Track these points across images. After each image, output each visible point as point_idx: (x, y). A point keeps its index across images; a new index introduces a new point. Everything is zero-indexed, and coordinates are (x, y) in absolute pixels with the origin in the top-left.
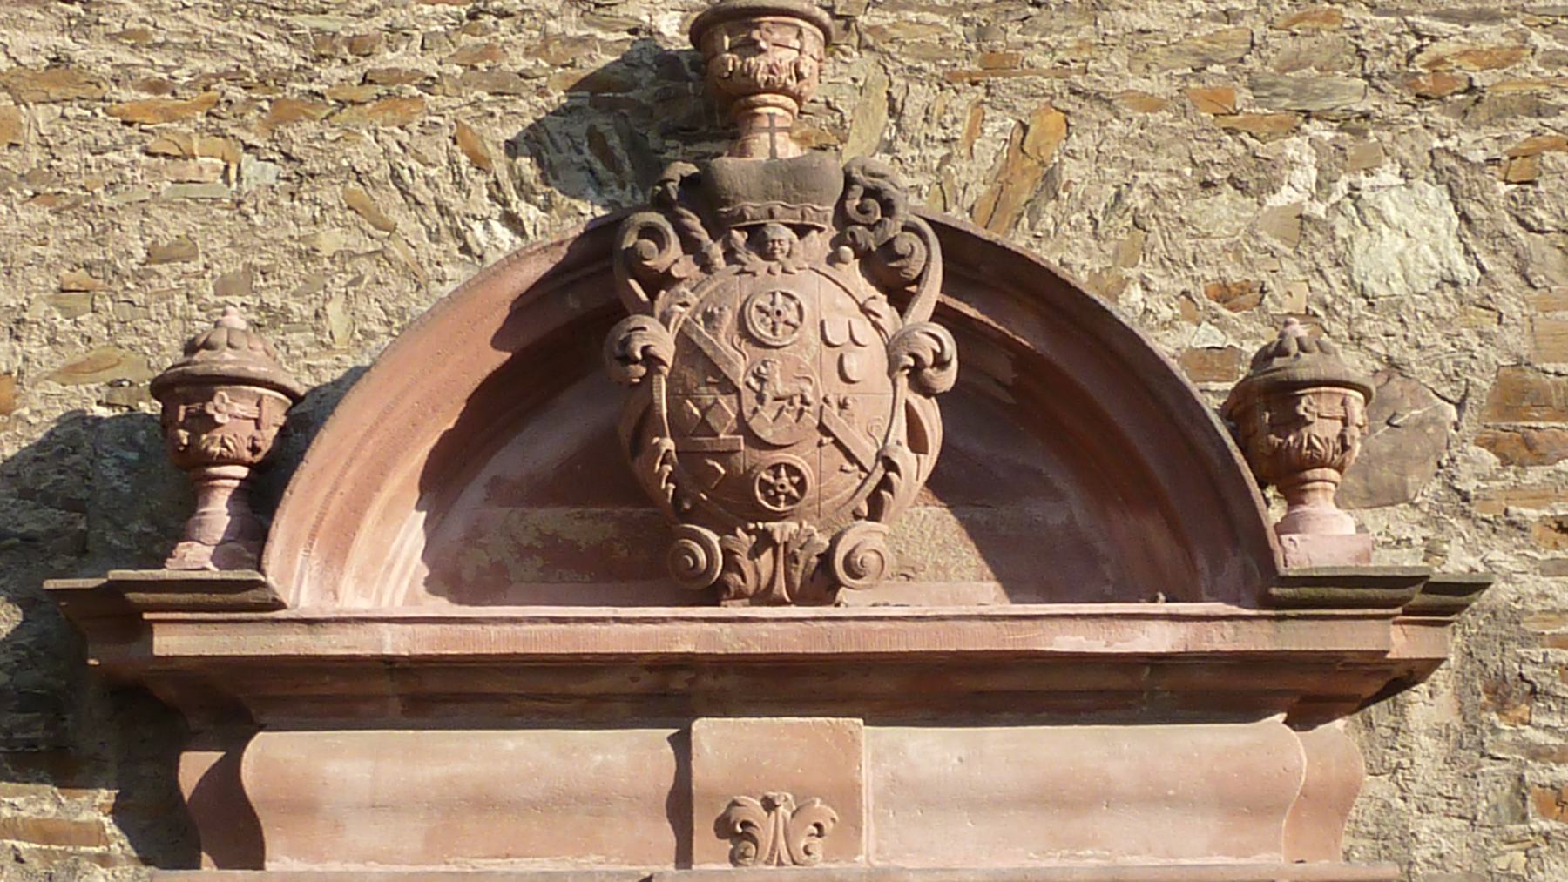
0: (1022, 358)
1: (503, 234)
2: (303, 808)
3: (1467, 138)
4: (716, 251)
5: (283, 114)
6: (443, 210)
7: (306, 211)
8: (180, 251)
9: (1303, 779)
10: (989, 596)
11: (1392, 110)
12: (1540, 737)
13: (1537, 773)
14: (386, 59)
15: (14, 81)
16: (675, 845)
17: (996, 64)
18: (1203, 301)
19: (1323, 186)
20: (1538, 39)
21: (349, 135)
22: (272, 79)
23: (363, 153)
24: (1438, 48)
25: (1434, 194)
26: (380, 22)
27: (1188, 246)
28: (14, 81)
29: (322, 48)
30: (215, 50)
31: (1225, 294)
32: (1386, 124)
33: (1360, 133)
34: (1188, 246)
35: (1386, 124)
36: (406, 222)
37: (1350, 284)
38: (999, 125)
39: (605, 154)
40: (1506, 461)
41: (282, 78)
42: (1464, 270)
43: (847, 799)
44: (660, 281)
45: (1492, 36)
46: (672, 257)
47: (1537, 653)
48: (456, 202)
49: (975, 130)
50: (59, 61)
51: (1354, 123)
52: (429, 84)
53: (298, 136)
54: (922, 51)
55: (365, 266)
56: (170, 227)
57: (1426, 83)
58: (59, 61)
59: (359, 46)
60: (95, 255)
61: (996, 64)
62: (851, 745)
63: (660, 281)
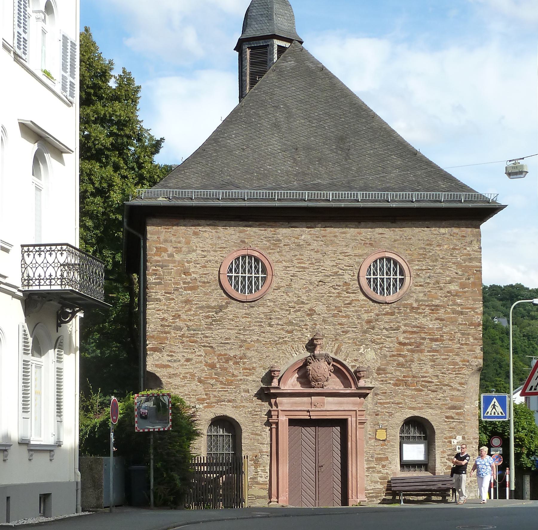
1: (295, 355)
2: (281, 403)
4: (315, 360)
5: (276, 344)
8: (268, 356)
10: (342, 387)
11: (370, 344)
13: (378, 401)
14: (285, 339)
17: (336, 340)
19: (364, 351)
21: (282, 346)
22: (276, 341)
23: (283, 348)
25: (373, 351)
29: (280, 338)
31: (355, 360)
38: (337, 345)
39: (304, 348)
41: (276, 341)
42: (375, 358)
43: (324, 403)
44: (310, 363)
45: (379, 337)
46: (311, 361)
48: (291, 352)
50: (258, 339)
51: (367, 345)
52: (289, 341)
54: (330, 338)
56: (267, 354)
58: (258, 339)
59: (283, 338)
62: (324, 399)
63: (310, 363)
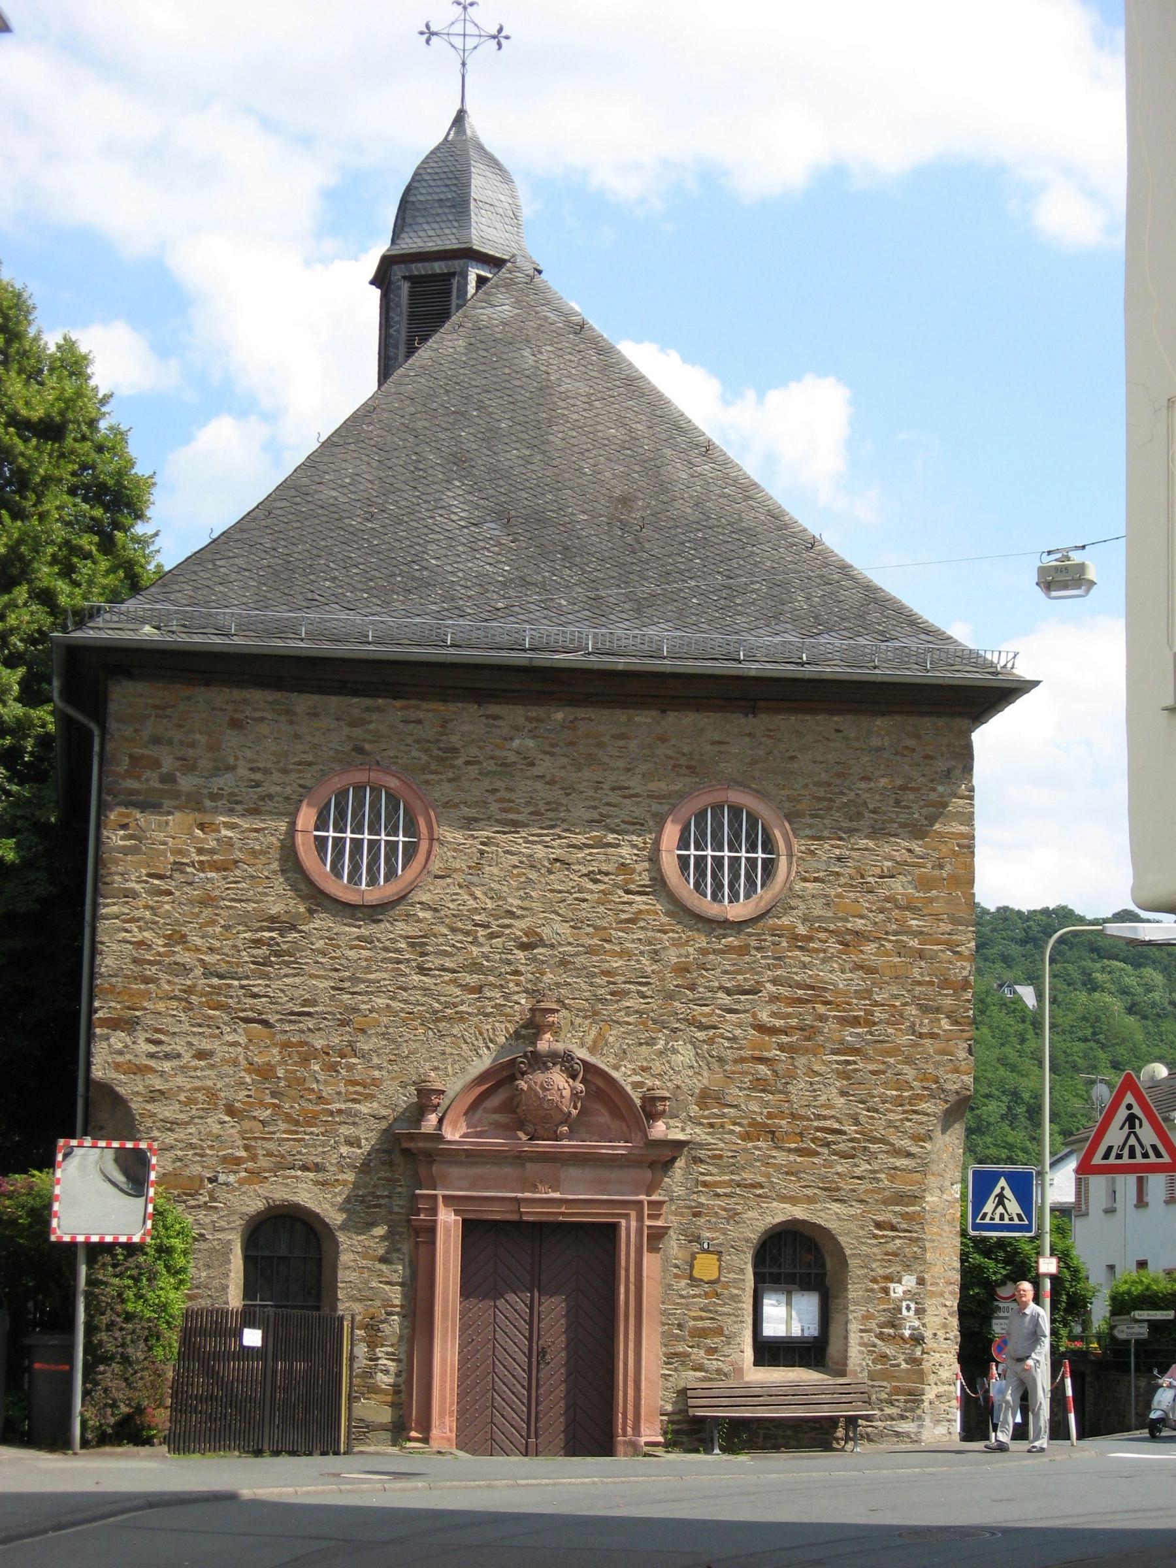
0: (598, 1088)
3: (699, 1034)
5: (438, 1020)
6: (473, 1045)
7: (443, 1044)
9: (797, 1357)
11: (683, 1027)
12: (703, 1171)
15: (197, 910)
16: (1130, 881)
18: (638, 1070)
20: (718, 1011)
21: (452, 1027)
23: (455, 1031)
24: (695, 1013)
25: (690, 1047)
26: (459, 999)
27: (635, 1057)
28: (197, 910)
30: (423, 1005)
31: (644, 1069)
32: (681, 1030)
33: (675, 1032)
34: (635, 1057)
35: (681, 1030)
36: (464, 1046)
37: (670, 1067)
40: (701, 1109)
47: (703, 1152)
48: (476, 1043)
49: (590, 1029)
51: (675, 1030)
53: (442, 1025)
55: (456, 1057)
56: (414, 1046)
57: (691, 1021)
58: (388, 1006)
59: (455, 1005)
60: (396, 1052)
61: (596, 1013)
